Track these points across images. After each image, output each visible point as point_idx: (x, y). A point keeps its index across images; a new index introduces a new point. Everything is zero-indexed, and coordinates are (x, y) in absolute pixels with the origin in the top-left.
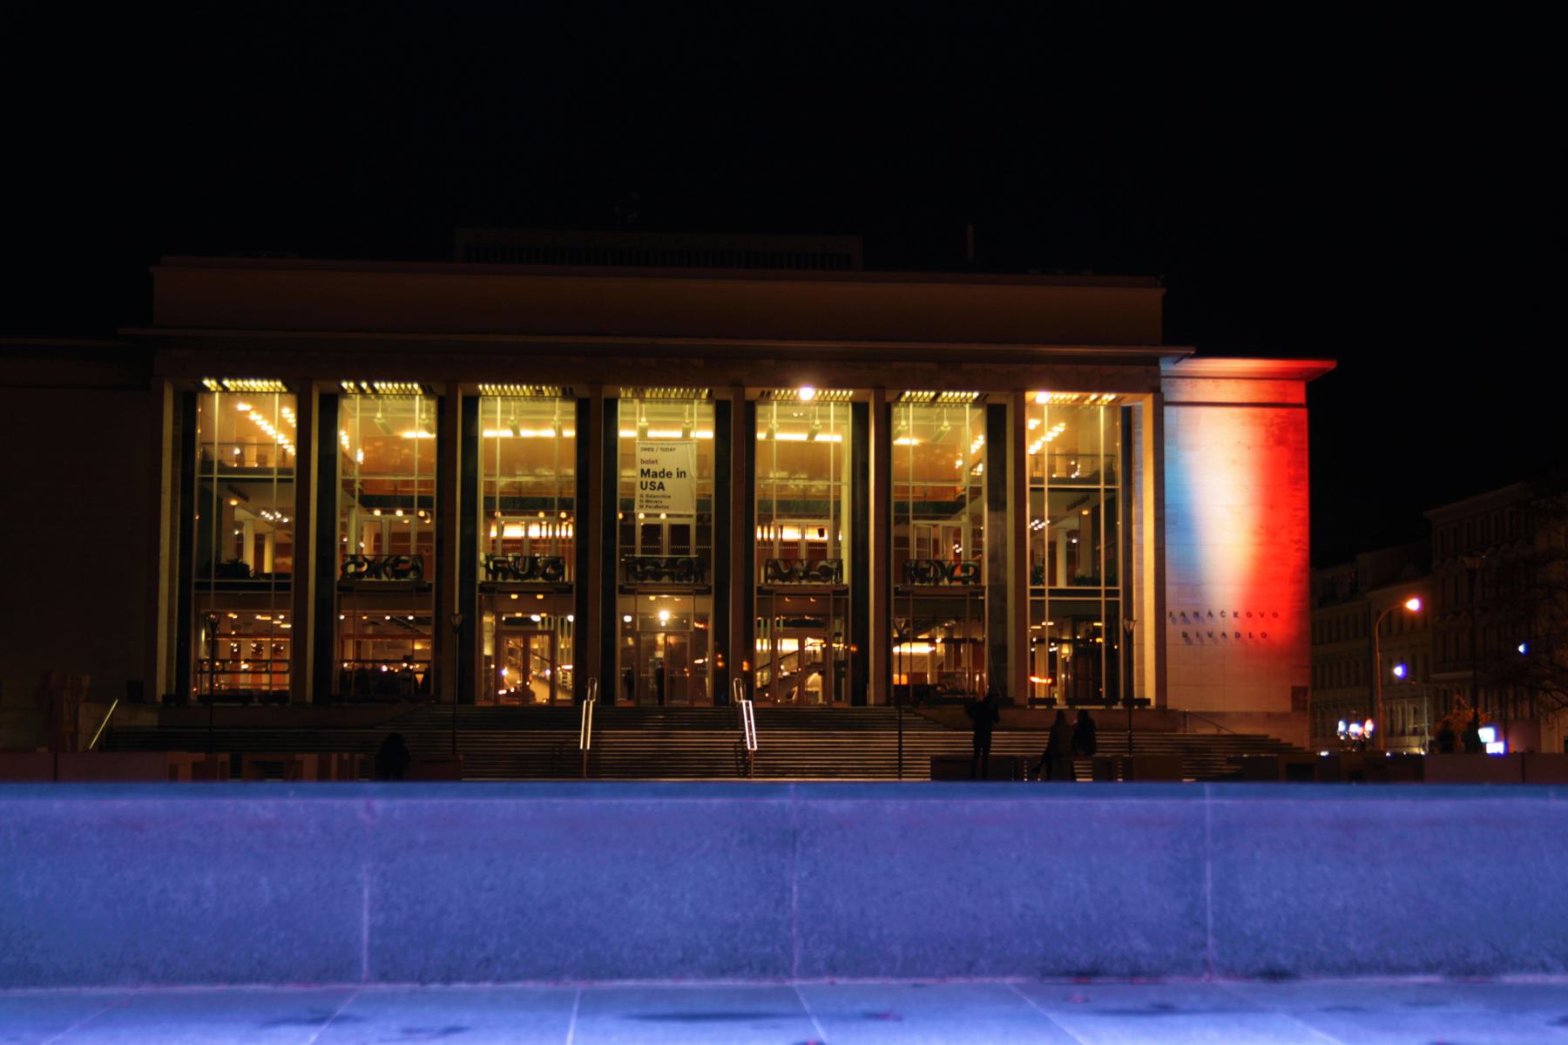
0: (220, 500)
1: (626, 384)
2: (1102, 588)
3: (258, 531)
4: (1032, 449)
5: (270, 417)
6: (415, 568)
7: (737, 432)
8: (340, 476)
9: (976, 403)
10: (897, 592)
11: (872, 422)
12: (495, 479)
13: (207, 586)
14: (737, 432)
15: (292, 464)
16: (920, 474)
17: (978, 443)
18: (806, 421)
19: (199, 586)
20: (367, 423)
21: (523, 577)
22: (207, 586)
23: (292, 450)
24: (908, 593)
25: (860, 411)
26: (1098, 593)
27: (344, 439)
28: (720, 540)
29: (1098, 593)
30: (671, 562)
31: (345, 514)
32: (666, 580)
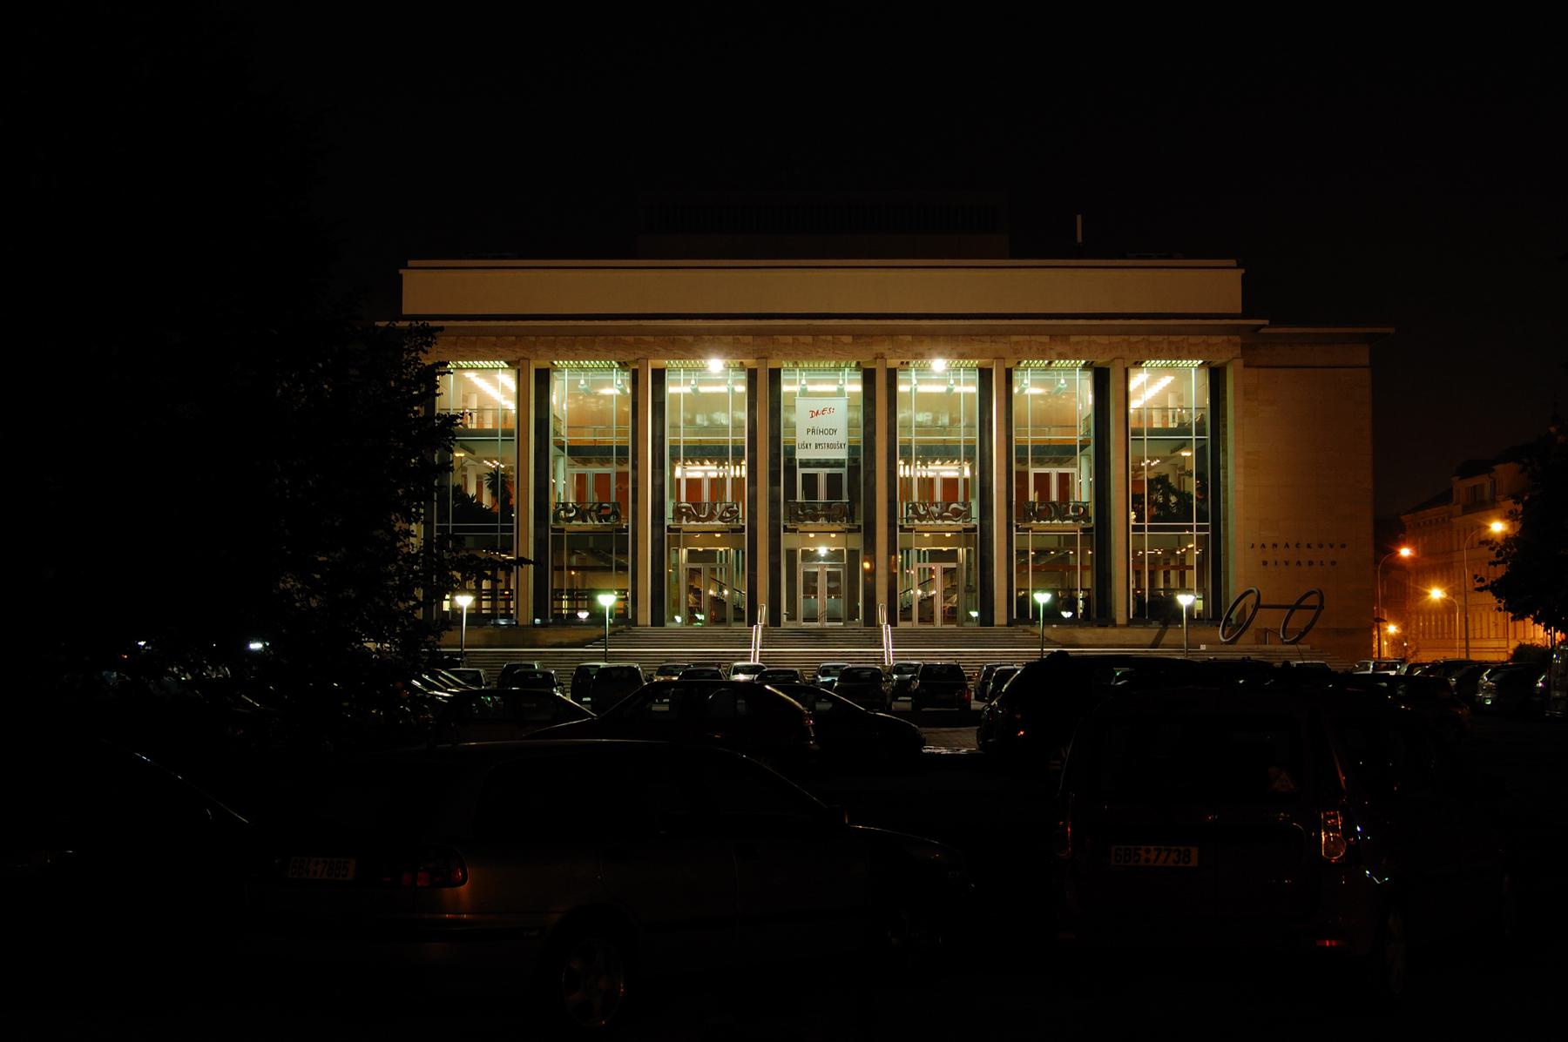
0: (893, 713)
1: (787, 356)
2: (1146, 524)
3: (472, 472)
4: (1135, 404)
5: (495, 383)
6: (615, 513)
7: (879, 393)
8: (552, 437)
9: (1085, 367)
10: (670, 529)
11: (995, 385)
12: (679, 434)
13: (1142, 528)
14: (879, 393)
15: (513, 424)
16: (1038, 427)
17: (1089, 398)
18: (937, 383)
19: (1135, 528)
20: (573, 384)
21: (703, 520)
22: (1142, 528)
23: (512, 406)
24: (678, 530)
25: (985, 376)
26: (1151, 529)
27: (554, 399)
28: (855, 491)
29: (494, 529)
30: (827, 506)
31: (555, 461)
32: (822, 521)
